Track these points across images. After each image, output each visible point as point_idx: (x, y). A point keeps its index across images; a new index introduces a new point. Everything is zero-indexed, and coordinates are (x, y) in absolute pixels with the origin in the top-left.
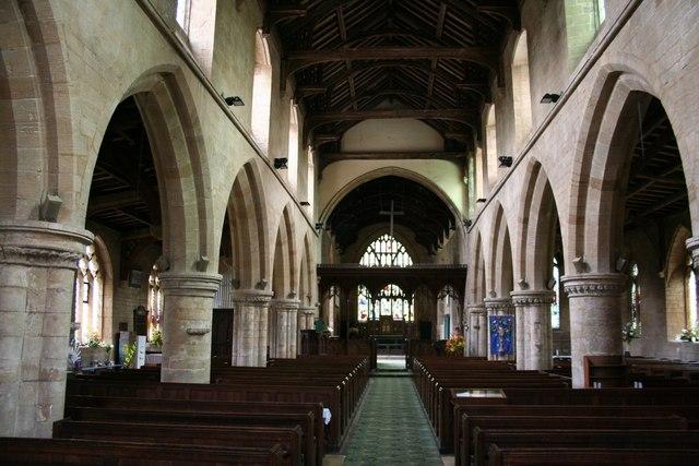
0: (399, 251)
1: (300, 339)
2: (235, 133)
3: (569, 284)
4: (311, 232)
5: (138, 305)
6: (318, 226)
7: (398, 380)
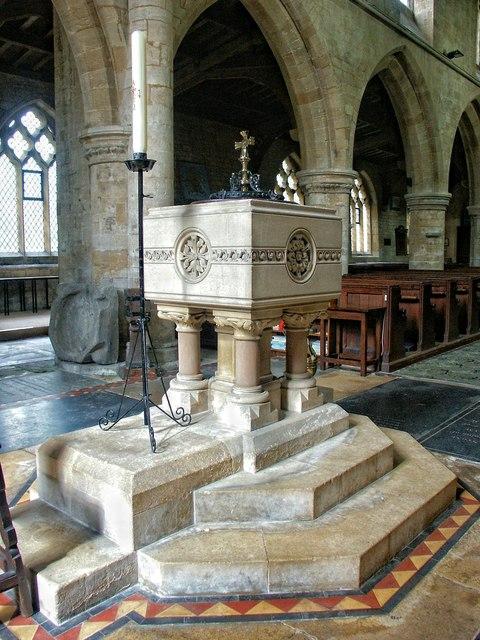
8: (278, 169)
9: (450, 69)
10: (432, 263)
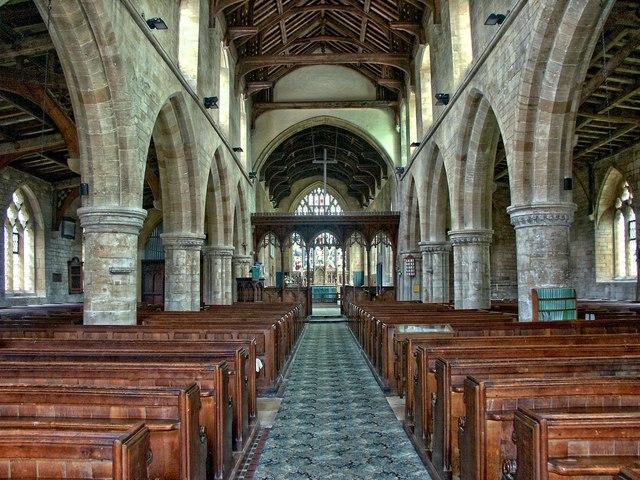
0: (332, 203)
1: (235, 286)
2: (159, 61)
3: (517, 214)
4: (244, 183)
5: (71, 257)
6: (252, 175)
7: (333, 324)
10: (119, 312)
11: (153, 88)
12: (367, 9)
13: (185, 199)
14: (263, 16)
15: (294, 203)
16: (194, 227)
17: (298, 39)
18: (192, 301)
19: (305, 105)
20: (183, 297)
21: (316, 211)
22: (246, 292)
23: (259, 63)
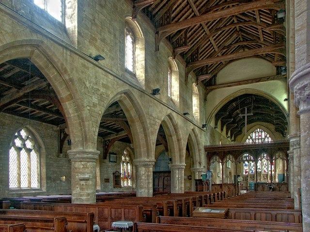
0: (266, 137)
8: (123, 154)
9: (95, 67)
10: (84, 198)
11: (102, 90)
12: (258, 20)
13: (142, 142)
14: (198, 37)
15: (244, 139)
16: (148, 156)
17: (225, 46)
18: (148, 192)
19: (234, 84)
20: (143, 190)
21: (257, 141)
22: (199, 187)
23: (200, 64)
